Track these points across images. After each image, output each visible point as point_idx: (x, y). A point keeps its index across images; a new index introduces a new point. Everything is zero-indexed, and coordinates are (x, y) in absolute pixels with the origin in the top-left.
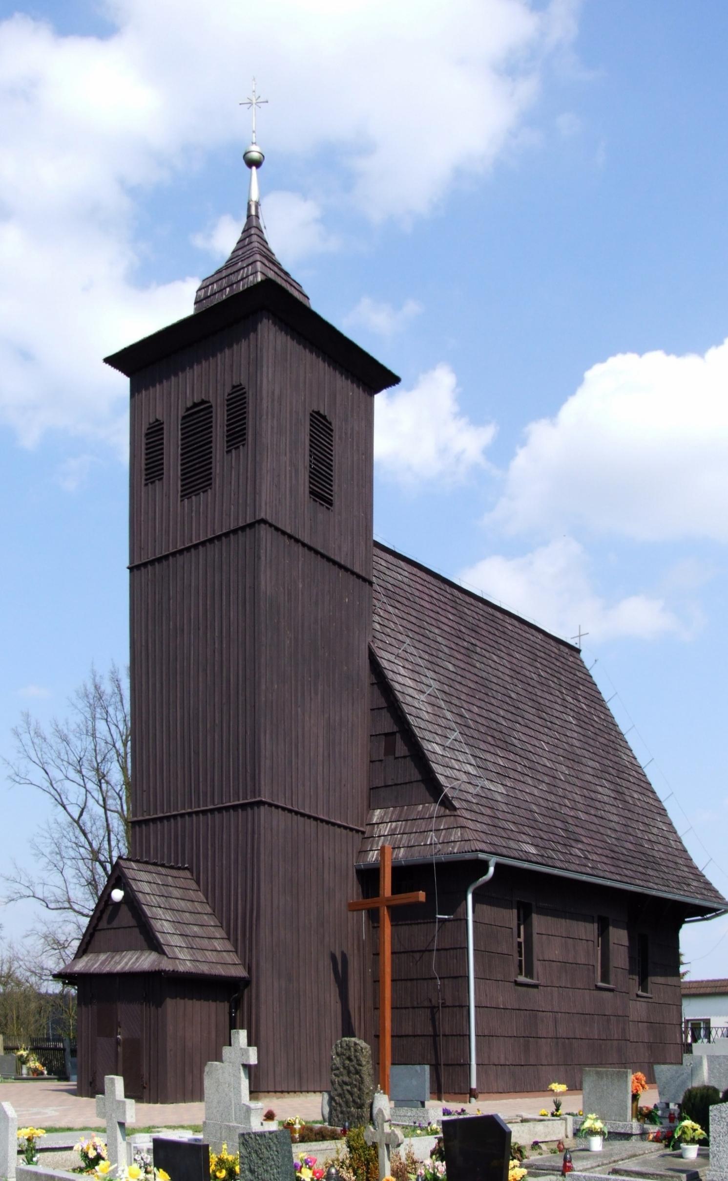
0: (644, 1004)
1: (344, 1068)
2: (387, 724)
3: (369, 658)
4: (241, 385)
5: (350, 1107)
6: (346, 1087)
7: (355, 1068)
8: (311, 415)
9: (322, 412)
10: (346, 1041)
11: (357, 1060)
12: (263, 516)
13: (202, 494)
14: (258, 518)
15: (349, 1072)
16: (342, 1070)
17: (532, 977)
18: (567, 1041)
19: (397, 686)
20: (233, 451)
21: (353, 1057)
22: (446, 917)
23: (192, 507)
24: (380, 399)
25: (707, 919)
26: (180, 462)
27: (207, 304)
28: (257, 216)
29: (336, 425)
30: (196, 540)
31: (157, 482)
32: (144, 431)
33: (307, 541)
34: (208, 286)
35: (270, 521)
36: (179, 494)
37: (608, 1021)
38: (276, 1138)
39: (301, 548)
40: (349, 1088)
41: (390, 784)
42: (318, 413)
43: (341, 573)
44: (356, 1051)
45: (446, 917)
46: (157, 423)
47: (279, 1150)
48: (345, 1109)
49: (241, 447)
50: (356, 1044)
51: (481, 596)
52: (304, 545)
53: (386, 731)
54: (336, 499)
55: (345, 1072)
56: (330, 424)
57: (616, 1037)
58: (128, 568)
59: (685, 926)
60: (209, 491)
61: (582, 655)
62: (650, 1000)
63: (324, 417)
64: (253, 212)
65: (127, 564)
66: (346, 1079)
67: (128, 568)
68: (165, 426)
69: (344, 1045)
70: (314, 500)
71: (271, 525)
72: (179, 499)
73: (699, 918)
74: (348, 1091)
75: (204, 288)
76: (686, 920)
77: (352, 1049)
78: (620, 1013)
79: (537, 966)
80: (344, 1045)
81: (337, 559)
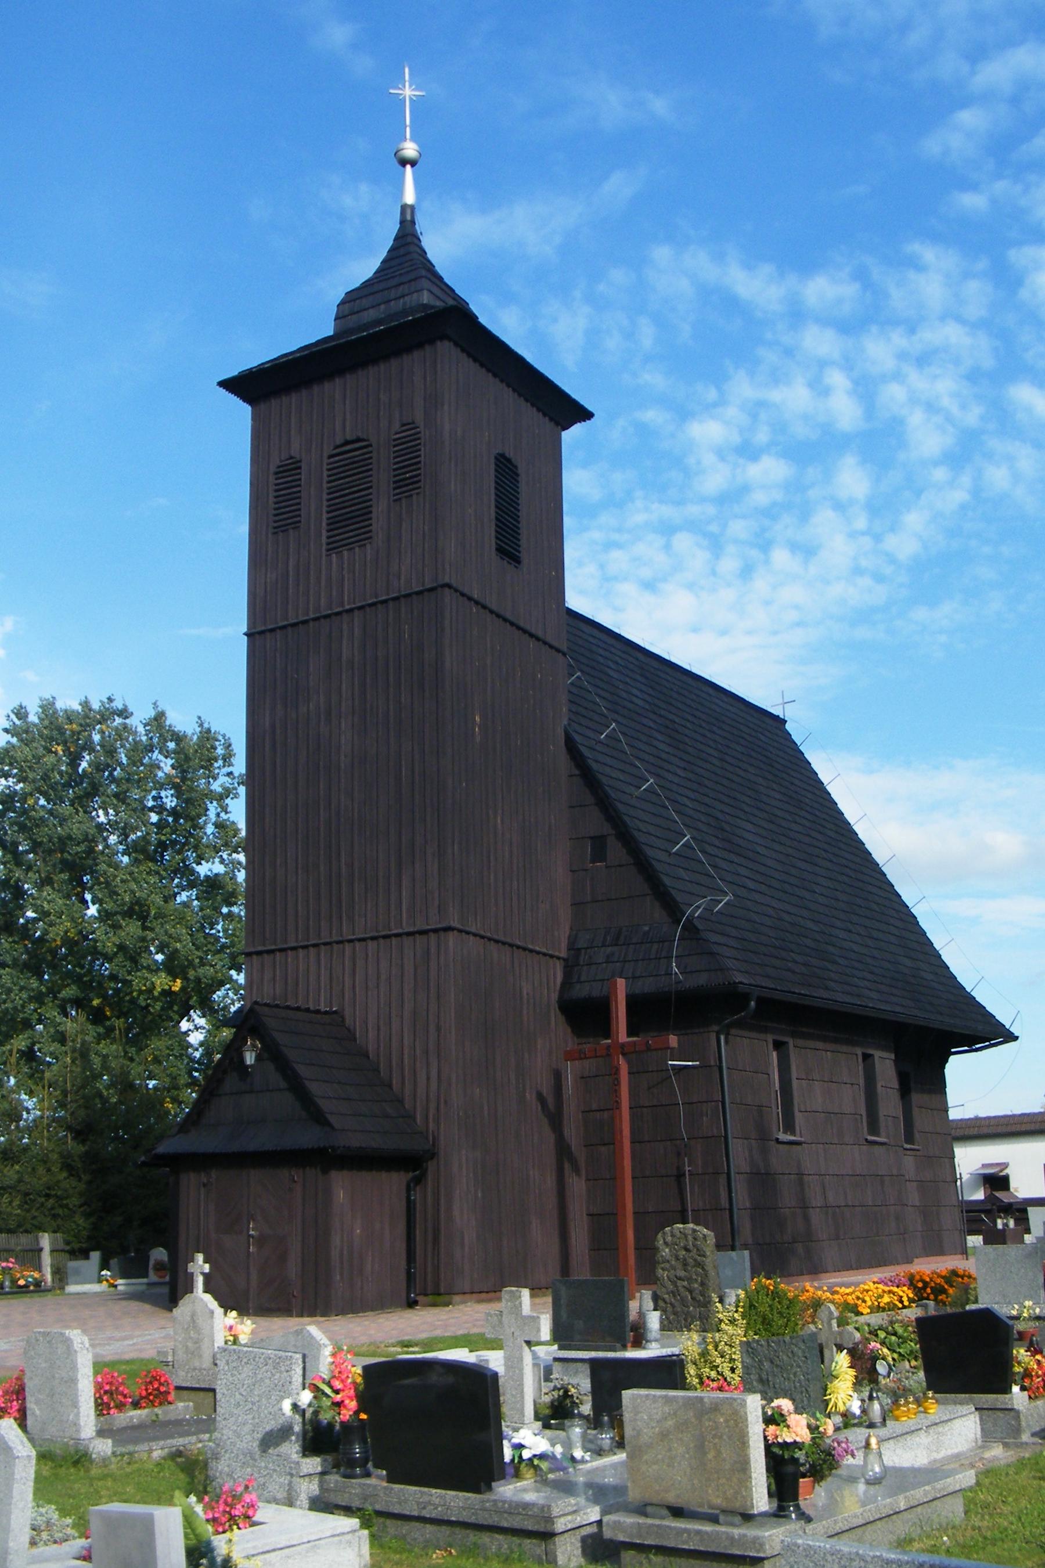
0: (911, 1159)
1: (677, 1259)
2: (595, 823)
3: (566, 744)
4: (413, 423)
5: (688, 1307)
6: (679, 1283)
7: (695, 1260)
8: (496, 458)
9: (507, 455)
10: (679, 1228)
11: (698, 1250)
12: (447, 580)
13: (357, 549)
14: (441, 582)
15: (685, 1264)
16: (673, 1263)
17: (793, 1133)
18: (837, 1210)
19: (604, 780)
20: (404, 501)
21: (691, 1247)
22: (690, 1063)
23: (343, 563)
24: (572, 436)
25: (977, 1050)
26: (325, 509)
27: (352, 321)
28: (413, 222)
29: (522, 469)
30: (348, 604)
31: (291, 531)
32: (273, 469)
33: (494, 607)
34: (354, 300)
35: (455, 585)
36: (324, 547)
37: (882, 1182)
38: (804, 1341)
39: (489, 614)
40: (685, 1283)
41: (600, 899)
42: (503, 456)
43: (532, 644)
44: (695, 1239)
45: (690, 1063)
46: (290, 461)
47: (808, 1355)
48: (679, 1309)
49: (415, 497)
50: (694, 1231)
51: (667, 657)
52: (491, 612)
53: (592, 835)
54: (524, 556)
55: (679, 1265)
56: (516, 467)
57: (892, 1202)
58: (245, 634)
59: (952, 1058)
60: (368, 546)
61: (788, 726)
62: (918, 1153)
63: (509, 460)
64: (409, 218)
65: (244, 629)
66: (682, 1273)
67: (245, 634)
68: (303, 465)
69: (678, 1234)
70: (501, 558)
71: (456, 590)
72: (324, 553)
73: (966, 1048)
74: (684, 1287)
75: (349, 302)
76: (953, 1050)
77: (690, 1238)
78: (895, 1172)
79: (799, 1118)
80: (678, 1234)
81: (528, 627)
